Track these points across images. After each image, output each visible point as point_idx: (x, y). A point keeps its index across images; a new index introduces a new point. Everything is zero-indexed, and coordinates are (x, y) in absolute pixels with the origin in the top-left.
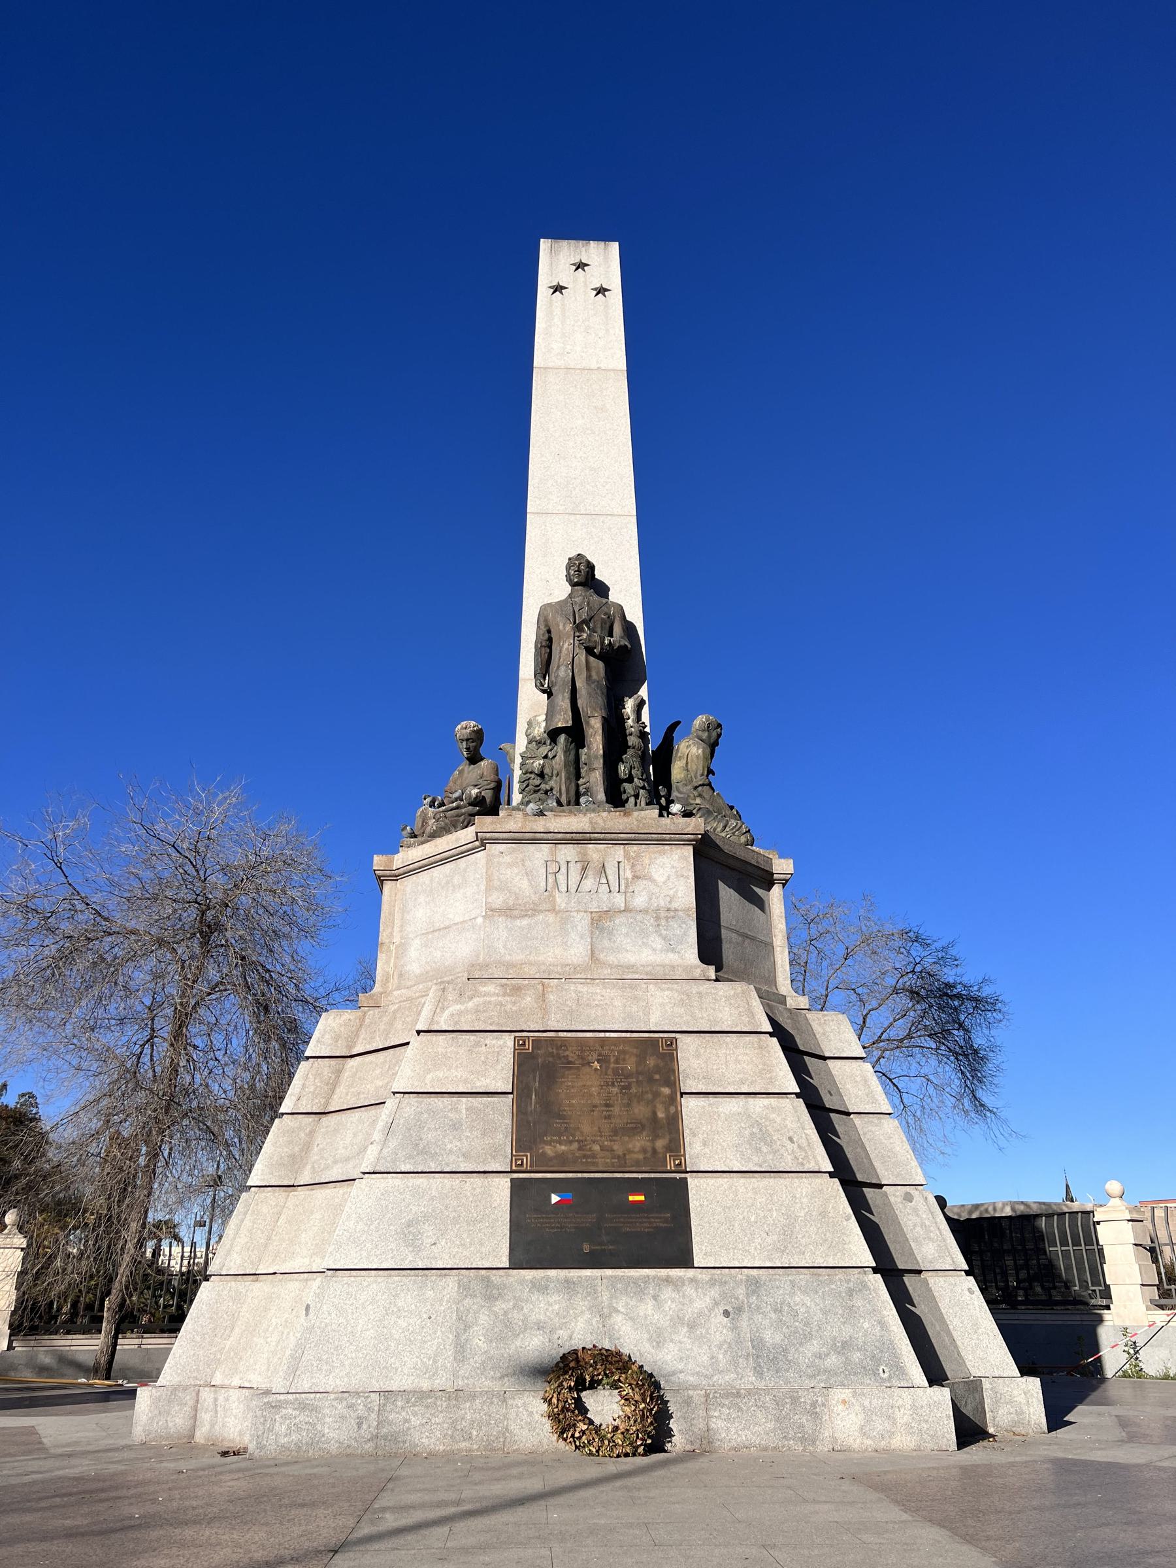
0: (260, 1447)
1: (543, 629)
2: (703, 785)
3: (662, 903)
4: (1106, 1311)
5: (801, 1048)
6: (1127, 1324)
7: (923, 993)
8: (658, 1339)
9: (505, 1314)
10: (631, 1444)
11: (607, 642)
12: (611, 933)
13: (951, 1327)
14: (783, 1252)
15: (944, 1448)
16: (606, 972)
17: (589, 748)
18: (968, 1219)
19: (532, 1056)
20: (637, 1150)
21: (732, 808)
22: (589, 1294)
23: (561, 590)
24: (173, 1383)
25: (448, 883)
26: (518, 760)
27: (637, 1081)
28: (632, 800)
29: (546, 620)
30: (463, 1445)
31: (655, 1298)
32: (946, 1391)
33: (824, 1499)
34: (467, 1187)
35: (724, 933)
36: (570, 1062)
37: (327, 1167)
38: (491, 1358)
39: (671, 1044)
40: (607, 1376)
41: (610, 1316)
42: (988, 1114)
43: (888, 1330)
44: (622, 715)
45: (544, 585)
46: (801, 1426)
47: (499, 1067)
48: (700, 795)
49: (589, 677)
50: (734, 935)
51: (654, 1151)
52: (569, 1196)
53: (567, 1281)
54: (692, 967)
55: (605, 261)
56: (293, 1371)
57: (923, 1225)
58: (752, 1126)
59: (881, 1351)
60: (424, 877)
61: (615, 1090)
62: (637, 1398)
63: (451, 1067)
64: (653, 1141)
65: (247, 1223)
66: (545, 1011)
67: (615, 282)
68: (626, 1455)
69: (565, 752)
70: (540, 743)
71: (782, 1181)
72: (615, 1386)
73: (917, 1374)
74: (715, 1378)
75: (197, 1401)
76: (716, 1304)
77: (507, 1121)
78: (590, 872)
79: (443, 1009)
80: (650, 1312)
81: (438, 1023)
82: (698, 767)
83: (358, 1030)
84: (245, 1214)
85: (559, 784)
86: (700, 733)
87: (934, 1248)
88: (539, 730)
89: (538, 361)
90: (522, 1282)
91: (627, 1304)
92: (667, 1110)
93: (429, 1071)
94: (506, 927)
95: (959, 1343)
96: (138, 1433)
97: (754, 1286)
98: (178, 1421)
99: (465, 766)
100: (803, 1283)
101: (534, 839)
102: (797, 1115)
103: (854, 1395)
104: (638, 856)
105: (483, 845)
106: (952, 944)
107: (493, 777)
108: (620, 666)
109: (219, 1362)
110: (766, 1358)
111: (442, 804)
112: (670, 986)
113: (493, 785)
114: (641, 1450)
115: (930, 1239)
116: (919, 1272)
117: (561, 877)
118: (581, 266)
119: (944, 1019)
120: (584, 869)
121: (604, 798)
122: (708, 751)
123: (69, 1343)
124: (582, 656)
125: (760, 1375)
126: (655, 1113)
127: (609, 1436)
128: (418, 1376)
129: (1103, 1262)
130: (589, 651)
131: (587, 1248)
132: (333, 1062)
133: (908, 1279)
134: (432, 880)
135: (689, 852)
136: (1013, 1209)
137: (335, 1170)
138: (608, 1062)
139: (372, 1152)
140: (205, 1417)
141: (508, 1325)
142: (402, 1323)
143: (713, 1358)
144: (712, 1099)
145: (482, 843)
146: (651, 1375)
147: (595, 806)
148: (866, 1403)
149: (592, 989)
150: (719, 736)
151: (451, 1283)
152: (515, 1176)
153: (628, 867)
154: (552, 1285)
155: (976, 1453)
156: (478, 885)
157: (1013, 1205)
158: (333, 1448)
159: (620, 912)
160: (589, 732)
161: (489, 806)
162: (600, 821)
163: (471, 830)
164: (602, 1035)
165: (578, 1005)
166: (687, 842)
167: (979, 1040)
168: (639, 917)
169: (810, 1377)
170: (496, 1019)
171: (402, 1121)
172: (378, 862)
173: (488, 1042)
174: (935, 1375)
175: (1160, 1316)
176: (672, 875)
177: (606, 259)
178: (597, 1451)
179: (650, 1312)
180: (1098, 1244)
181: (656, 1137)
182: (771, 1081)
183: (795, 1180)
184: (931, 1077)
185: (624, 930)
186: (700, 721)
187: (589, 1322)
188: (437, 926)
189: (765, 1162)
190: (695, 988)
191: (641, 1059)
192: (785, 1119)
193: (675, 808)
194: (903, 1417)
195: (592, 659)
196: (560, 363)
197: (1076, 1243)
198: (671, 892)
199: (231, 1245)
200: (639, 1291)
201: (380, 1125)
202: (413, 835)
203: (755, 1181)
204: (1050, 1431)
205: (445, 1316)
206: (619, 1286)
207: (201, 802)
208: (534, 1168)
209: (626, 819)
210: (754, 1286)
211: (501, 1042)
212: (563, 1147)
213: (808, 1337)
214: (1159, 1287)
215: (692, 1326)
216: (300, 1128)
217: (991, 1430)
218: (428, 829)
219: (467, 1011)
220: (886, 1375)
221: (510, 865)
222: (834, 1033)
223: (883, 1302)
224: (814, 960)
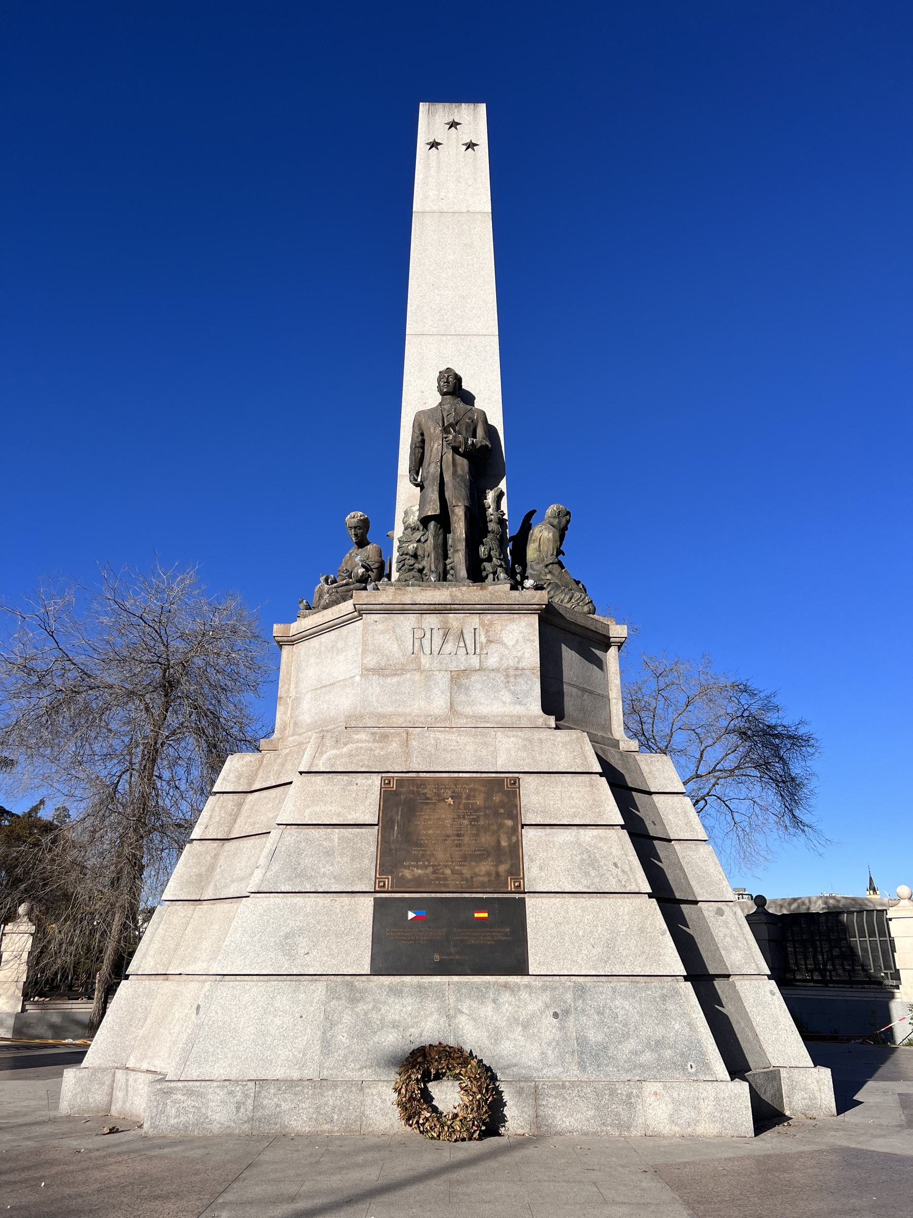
2: (552, 563)
3: (511, 663)
4: (896, 991)
5: (630, 785)
7: (749, 733)
9: (366, 1014)
10: (467, 1130)
11: (470, 442)
12: (467, 689)
13: (754, 1024)
14: (606, 962)
15: (743, 1135)
16: (462, 722)
17: (454, 533)
19: (396, 793)
20: (482, 873)
21: (578, 583)
22: (438, 997)
24: (95, 1065)
25: (333, 647)
26: (396, 544)
27: (485, 815)
28: (491, 576)
29: (420, 426)
30: (326, 1127)
31: (494, 1001)
32: (746, 1085)
33: (622, 1199)
34: (337, 905)
36: (428, 799)
38: (352, 1052)
39: (515, 783)
40: (450, 1070)
45: (419, 395)
47: (367, 803)
48: (550, 572)
49: (455, 473)
50: (575, 690)
51: (498, 874)
53: (420, 986)
55: (474, 120)
57: (732, 936)
59: (690, 1049)
60: (315, 642)
61: (466, 822)
62: (474, 1089)
63: (326, 803)
64: (497, 866)
65: (160, 931)
66: (408, 755)
68: (463, 1140)
69: (434, 537)
70: (415, 529)
71: (607, 900)
72: (457, 1077)
73: (720, 1069)
74: (544, 1071)
75: (113, 1081)
76: (547, 1007)
77: (373, 849)
78: (450, 638)
79: (322, 754)
80: (490, 1014)
81: (317, 765)
82: (549, 548)
83: (258, 770)
84: (159, 923)
85: (429, 563)
86: (552, 520)
87: (739, 952)
88: (414, 519)
90: (381, 986)
91: (470, 1006)
92: (509, 839)
94: (387, 681)
95: (761, 1038)
96: (64, 1107)
97: (581, 991)
98: (97, 1098)
99: (354, 550)
100: (623, 989)
101: (403, 610)
102: (621, 845)
104: (491, 623)
105: (361, 615)
106: (774, 694)
107: (377, 558)
108: (483, 462)
110: (589, 1054)
111: (334, 581)
112: (515, 733)
114: (476, 1135)
115: (738, 948)
116: (728, 976)
117: (426, 642)
118: (453, 125)
119: (769, 752)
120: (445, 635)
121: (466, 575)
122: (557, 534)
123: (70, 1006)
124: (449, 455)
125: (582, 1067)
126: (499, 842)
127: (449, 1123)
128: (289, 1067)
129: (894, 951)
130: (455, 450)
131: (437, 958)
133: (718, 984)
134: (321, 644)
135: (535, 619)
136: (826, 903)
137: (232, 889)
138: (461, 798)
140: (119, 1095)
141: (368, 1024)
142: (278, 1021)
143: (543, 1053)
144: (548, 830)
145: (360, 613)
146: (489, 1069)
148: (675, 1095)
149: (448, 736)
150: (568, 522)
151: (320, 986)
153: (483, 634)
154: (406, 990)
155: (772, 1139)
156: (356, 649)
157: (826, 900)
158: (215, 1128)
159: (476, 671)
160: (453, 519)
162: (459, 594)
163: (351, 602)
164: (456, 775)
165: (436, 749)
166: (532, 612)
167: (796, 769)
168: (492, 675)
169: (627, 1071)
171: (283, 849)
172: (277, 629)
173: (359, 781)
174: (737, 1067)
176: (520, 639)
177: (475, 118)
178: (438, 1136)
179: (490, 1014)
180: (890, 936)
181: (499, 862)
182: (600, 814)
183: (618, 900)
184: (756, 800)
185: (479, 686)
186: (552, 509)
187: (437, 1022)
188: (324, 683)
189: (592, 884)
190: (537, 735)
192: (611, 847)
193: (529, 583)
194: (707, 1107)
195: (457, 457)
196: (435, 208)
198: (520, 654)
199: (147, 950)
200: (480, 994)
202: (308, 608)
203: (584, 901)
205: (314, 1016)
206: (464, 990)
207: (163, 583)
208: (395, 889)
209: (481, 592)
210: (581, 991)
211: (370, 782)
212: (420, 871)
213: (626, 1036)
215: (526, 1026)
216: (207, 852)
218: (322, 602)
219: (342, 756)
220: (693, 1070)
221: (383, 632)
222: (659, 773)
223: (692, 1007)
224: (661, 706)
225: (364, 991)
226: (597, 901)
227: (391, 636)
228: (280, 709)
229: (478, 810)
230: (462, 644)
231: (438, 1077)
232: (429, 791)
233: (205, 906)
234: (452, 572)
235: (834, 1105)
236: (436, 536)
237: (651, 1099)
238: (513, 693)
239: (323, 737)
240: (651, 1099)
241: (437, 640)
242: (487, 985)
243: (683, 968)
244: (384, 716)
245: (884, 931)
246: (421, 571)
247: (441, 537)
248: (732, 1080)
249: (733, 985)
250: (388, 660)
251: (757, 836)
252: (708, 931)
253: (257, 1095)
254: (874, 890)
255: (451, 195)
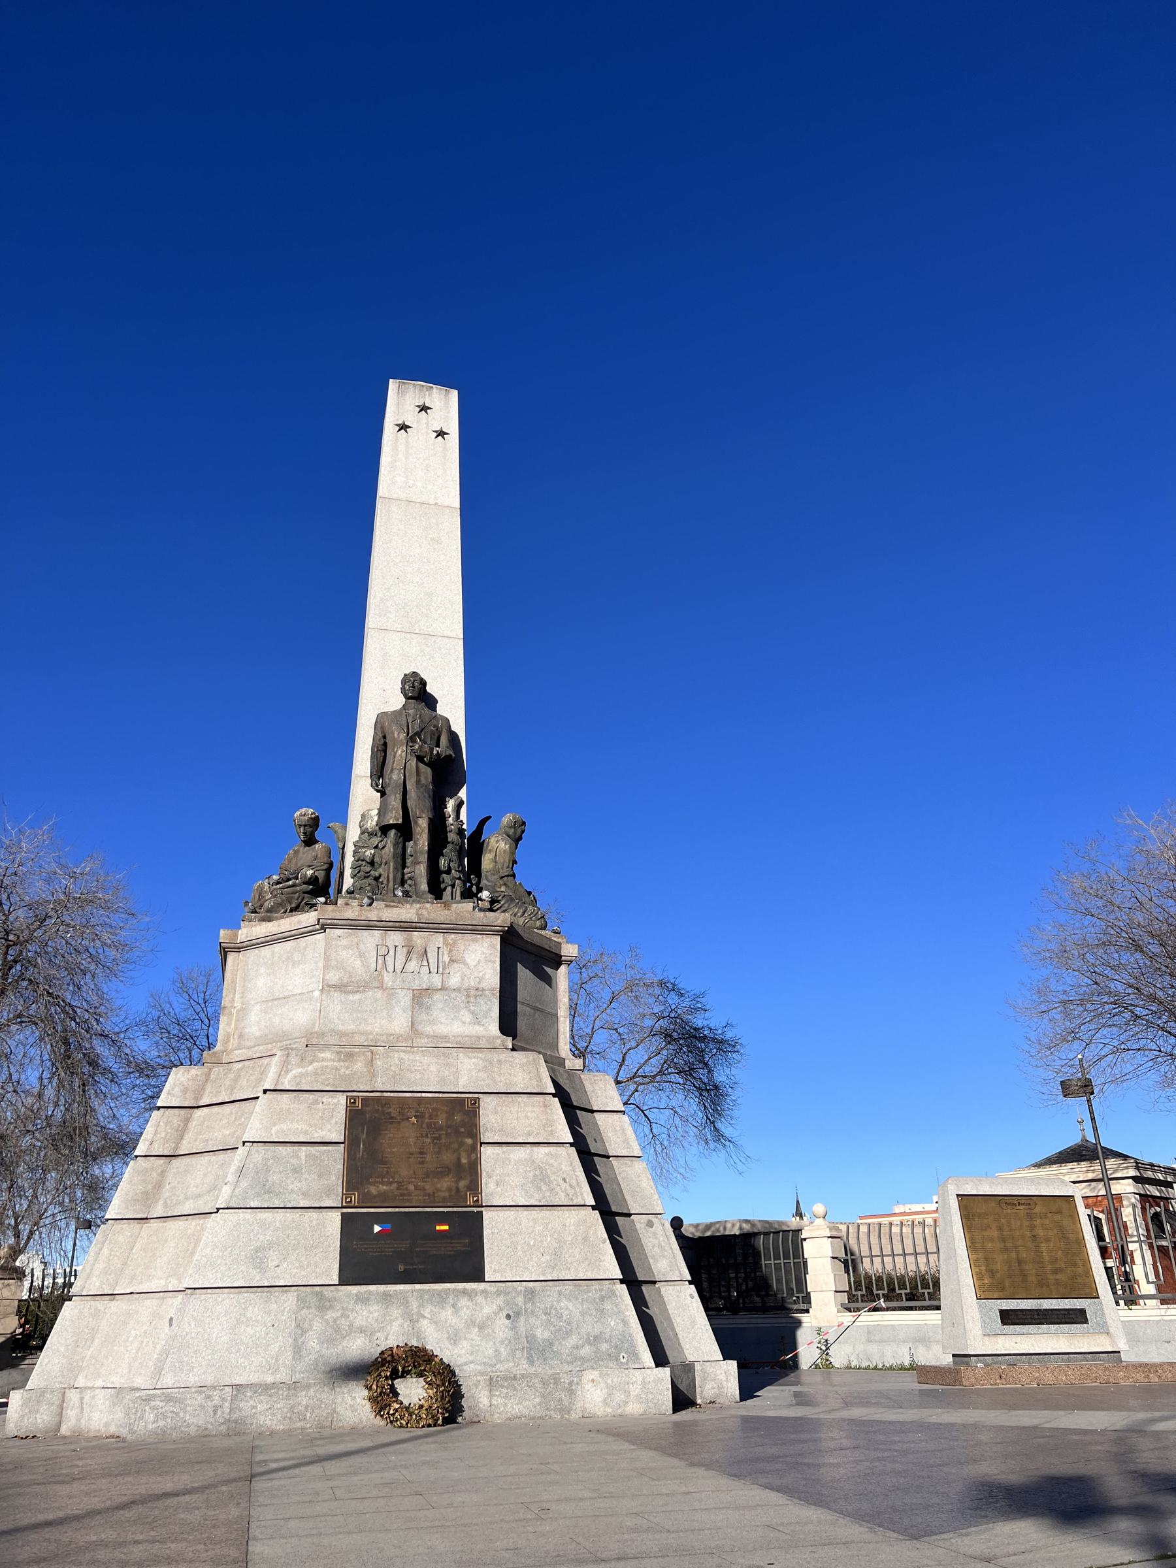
0: (132, 1432)
1: (380, 735)
6: (822, 1325)
7: (675, 1034)
8: (455, 1339)
9: (335, 1321)
12: (428, 1008)
16: (423, 1041)
17: (415, 843)
18: (700, 1238)
21: (529, 893)
22: (402, 1304)
23: (396, 701)
25: (288, 958)
28: (449, 889)
29: (382, 728)
30: (299, 1425)
31: (454, 1306)
35: (520, 1008)
37: (179, 1203)
40: (415, 1366)
41: (418, 1321)
42: (727, 1143)
43: (628, 1326)
44: (444, 814)
45: (379, 695)
46: (560, 1400)
47: (333, 1121)
49: (418, 782)
51: (458, 1189)
52: (388, 1226)
53: (385, 1294)
54: (494, 1038)
55: (445, 406)
56: (159, 1372)
57: (660, 1246)
58: (535, 1169)
60: (266, 951)
61: (428, 1140)
64: (457, 1182)
65: (105, 1251)
66: (373, 1075)
67: (453, 427)
68: (429, 1426)
70: (372, 834)
71: (555, 1213)
72: (420, 1375)
73: (647, 1358)
75: (63, 1401)
76: (501, 1309)
78: (414, 956)
79: (287, 1072)
80: (449, 1317)
82: (504, 859)
84: (103, 1243)
85: (386, 871)
87: (666, 1261)
88: (372, 823)
89: (382, 490)
90: (349, 1295)
92: (469, 1156)
93: (275, 1124)
97: (531, 1295)
98: (42, 1418)
101: (368, 926)
103: (601, 1375)
104: (455, 943)
106: (703, 995)
109: (81, 1369)
110: (535, 1350)
113: (325, 867)
114: (440, 1422)
116: (654, 1282)
117: (390, 959)
118: (424, 408)
119: (692, 1056)
120: (409, 953)
124: (413, 762)
125: (531, 1361)
126: (459, 1160)
128: (263, 1372)
129: (806, 1273)
130: (420, 759)
131: (401, 1268)
132: (182, 1111)
133: (644, 1288)
134: (273, 954)
135: (497, 940)
139: (226, 1191)
140: (71, 1414)
141: (337, 1330)
144: (505, 1148)
147: (420, 898)
148: (609, 1381)
150: (523, 832)
151: (291, 1297)
152: (345, 1210)
153: (446, 953)
155: (685, 1415)
156: (316, 963)
158: (193, 1430)
160: (416, 830)
161: (320, 888)
162: (425, 913)
164: (419, 1095)
165: (401, 1070)
167: (720, 1077)
168: (453, 995)
169: (569, 1363)
170: (331, 1081)
173: (325, 1100)
174: (660, 1359)
175: (848, 1317)
176: (481, 959)
177: (447, 404)
179: (449, 1317)
181: (460, 1178)
182: (552, 1133)
184: (678, 1110)
186: (507, 818)
187: (401, 1326)
190: (496, 1056)
191: (450, 1115)
194: (635, 1390)
195: (421, 765)
196: (403, 496)
197: (787, 1257)
200: (441, 1300)
201: (233, 1168)
203: (535, 1213)
204: (741, 1400)
210: (531, 1295)
211: (335, 1101)
213: (569, 1333)
214: (849, 1292)
215: (482, 1327)
216: (153, 1169)
217: (699, 1401)
221: (346, 947)
222: (601, 1091)
225: (332, 1301)
226: (546, 1213)
227: (356, 951)
228: (223, 1020)
229: (440, 1128)
230: (425, 963)
231: (405, 1374)
232: (394, 1111)
233: (154, 1224)
234: (409, 882)
235: (737, 1392)
236: (395, 845)
237: (589, 1386)
238: (473, 1013)
239: (288, 1055)
240: (589, 1386)
241: (401, 958)
242: (448, 1291)
243: (619, 1272)
244: (347, 1035)
245: (798, 1251)
246: (377, 879)
247: (401, 845)
248: (657, 1366)
249: (659, 1291)
250: (351, 976)
251: (677, 1151)
252: (639, 1241)
253: (234, 1398)
254: (801, 1216)
255: (419, 484)
